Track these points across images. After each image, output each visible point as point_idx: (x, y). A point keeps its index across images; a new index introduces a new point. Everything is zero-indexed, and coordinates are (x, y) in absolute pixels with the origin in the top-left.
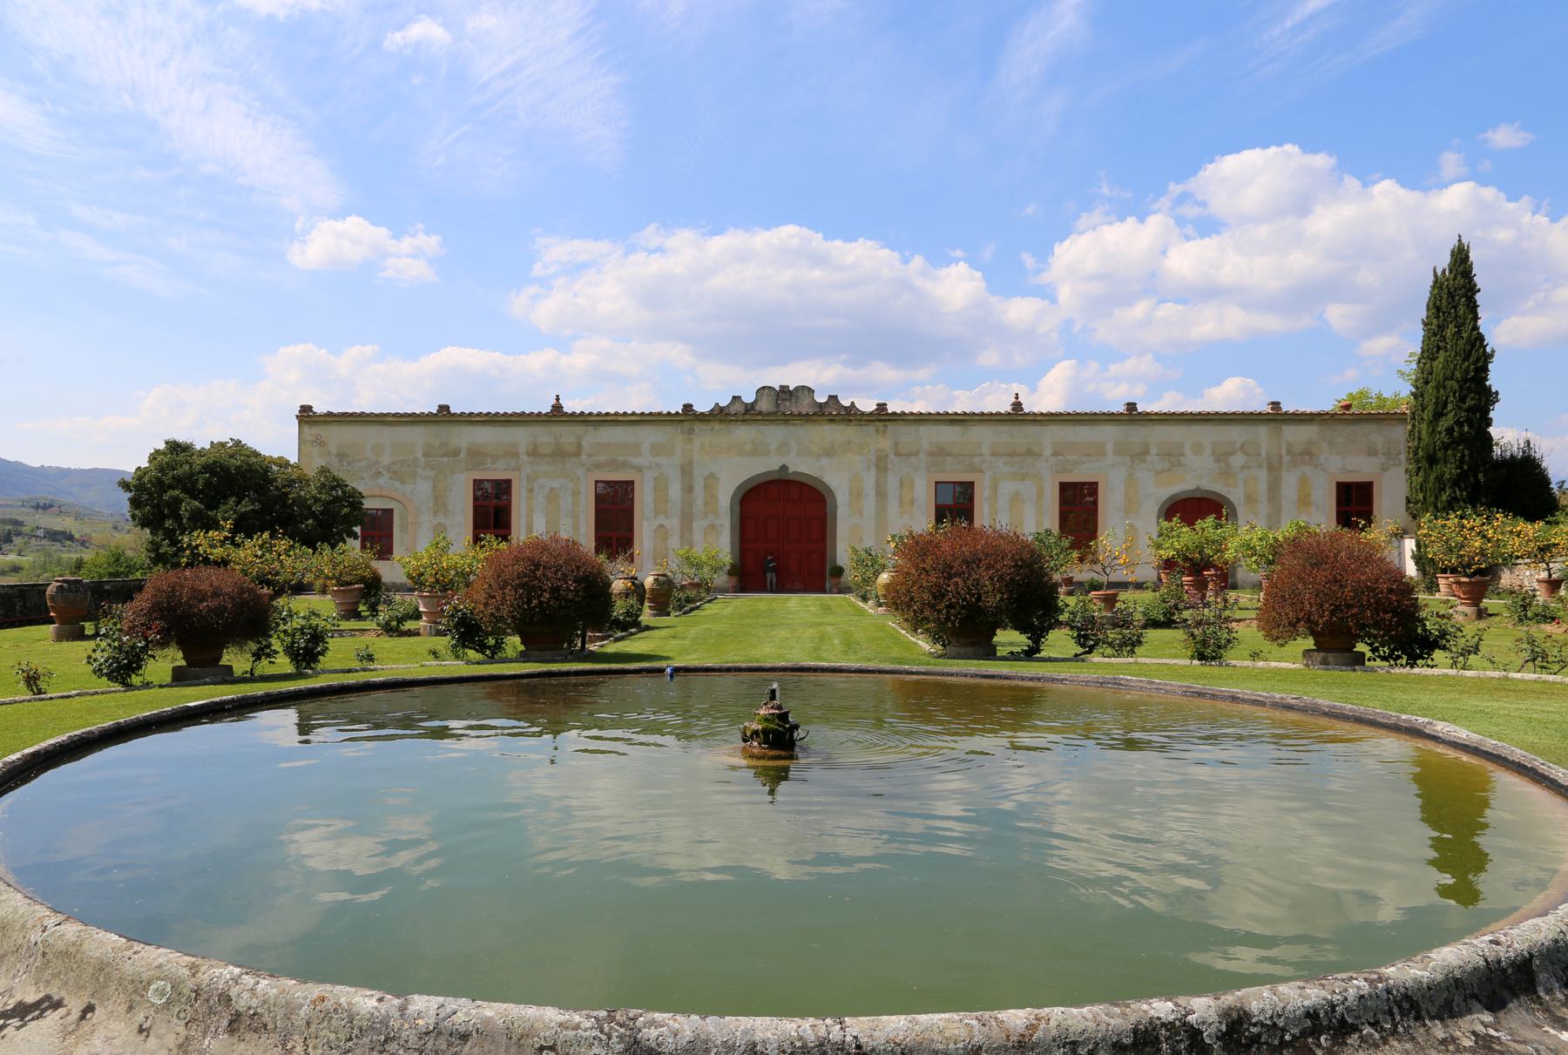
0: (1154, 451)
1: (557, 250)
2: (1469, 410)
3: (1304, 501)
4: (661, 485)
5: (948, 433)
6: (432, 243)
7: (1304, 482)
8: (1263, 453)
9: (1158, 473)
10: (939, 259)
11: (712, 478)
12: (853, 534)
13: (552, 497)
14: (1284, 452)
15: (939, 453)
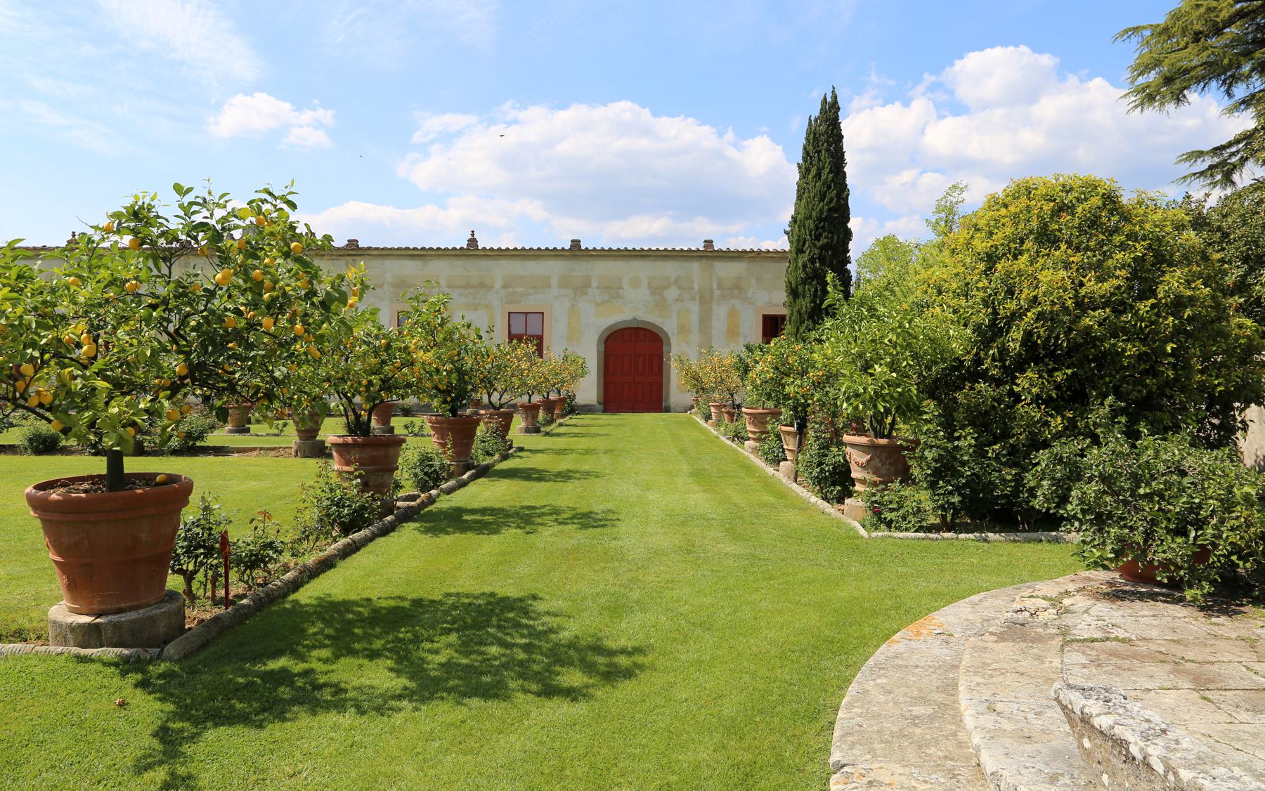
0: (595, 284)
1: (433, 123)
2: (822, 248)
5: (410, 268)
6: (327, 116)
7: (732, 314)
8: (696, 287)
9: (598, 305)
10: (746, 132)
12: (683, 358)
14: (715, 286)
15: (401, 284)
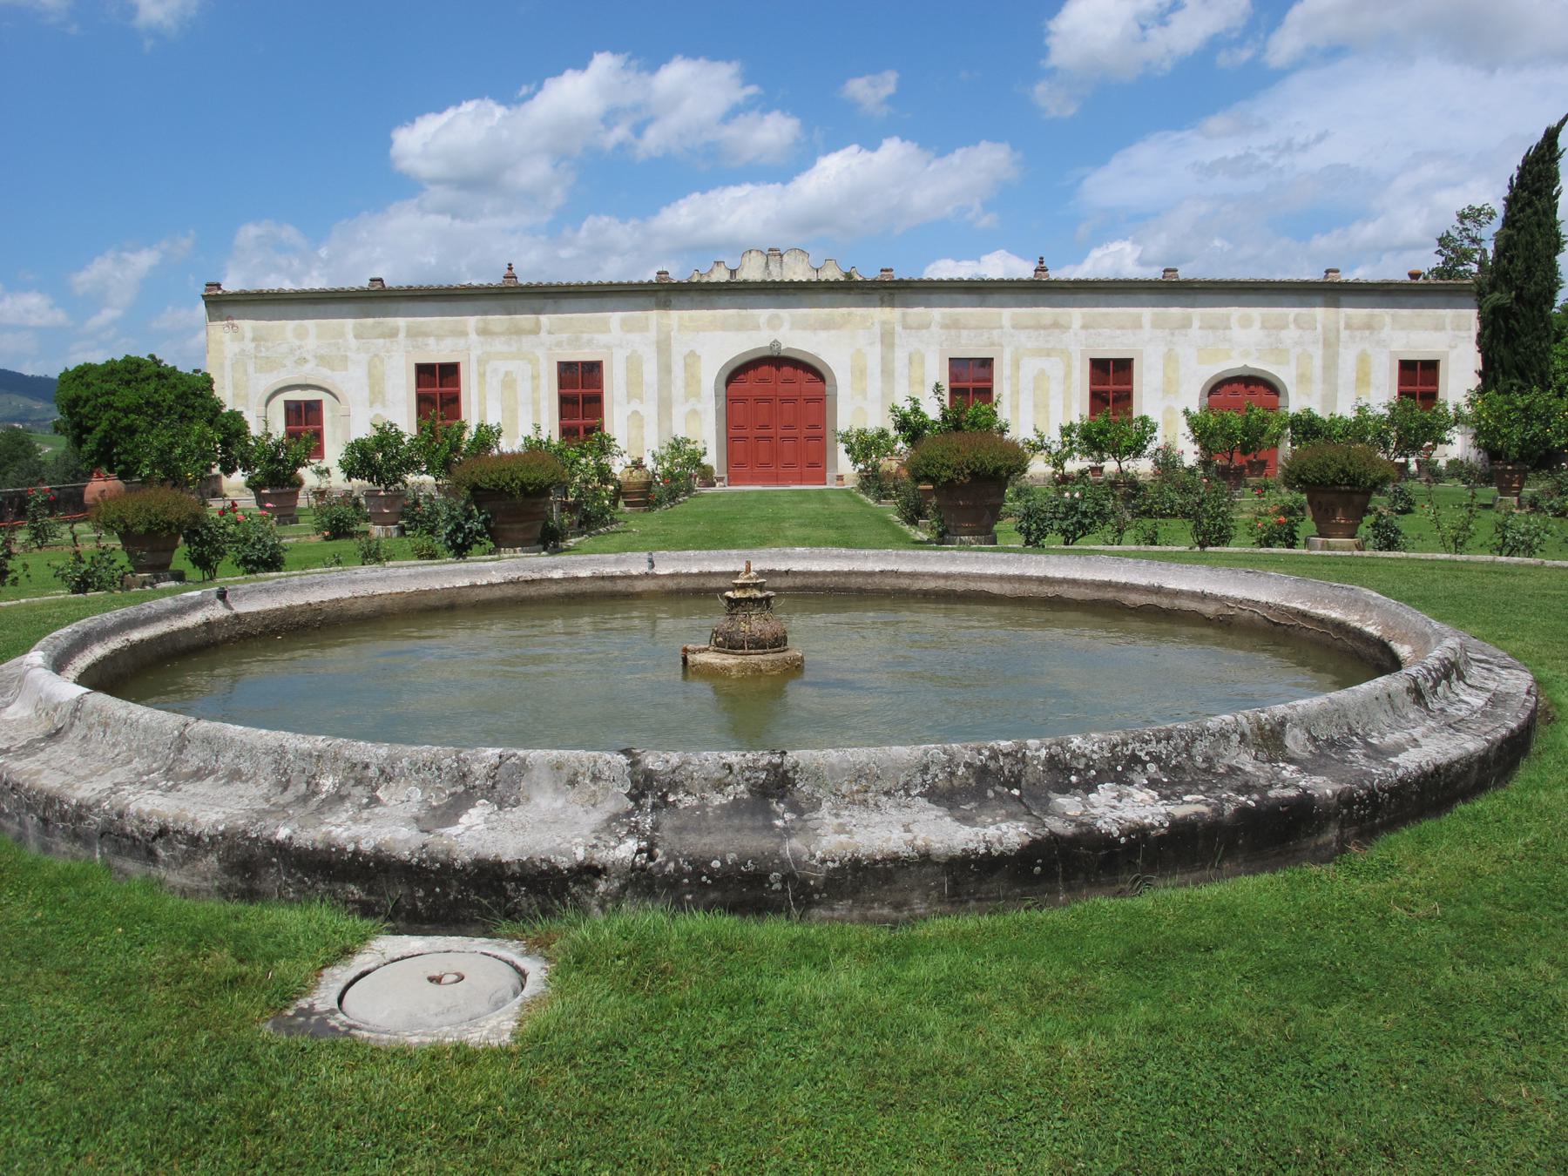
3: (1363, 380)
4: (634, 364)
7: (1363, 360)
11: (692, 358)
13: (508, 383)
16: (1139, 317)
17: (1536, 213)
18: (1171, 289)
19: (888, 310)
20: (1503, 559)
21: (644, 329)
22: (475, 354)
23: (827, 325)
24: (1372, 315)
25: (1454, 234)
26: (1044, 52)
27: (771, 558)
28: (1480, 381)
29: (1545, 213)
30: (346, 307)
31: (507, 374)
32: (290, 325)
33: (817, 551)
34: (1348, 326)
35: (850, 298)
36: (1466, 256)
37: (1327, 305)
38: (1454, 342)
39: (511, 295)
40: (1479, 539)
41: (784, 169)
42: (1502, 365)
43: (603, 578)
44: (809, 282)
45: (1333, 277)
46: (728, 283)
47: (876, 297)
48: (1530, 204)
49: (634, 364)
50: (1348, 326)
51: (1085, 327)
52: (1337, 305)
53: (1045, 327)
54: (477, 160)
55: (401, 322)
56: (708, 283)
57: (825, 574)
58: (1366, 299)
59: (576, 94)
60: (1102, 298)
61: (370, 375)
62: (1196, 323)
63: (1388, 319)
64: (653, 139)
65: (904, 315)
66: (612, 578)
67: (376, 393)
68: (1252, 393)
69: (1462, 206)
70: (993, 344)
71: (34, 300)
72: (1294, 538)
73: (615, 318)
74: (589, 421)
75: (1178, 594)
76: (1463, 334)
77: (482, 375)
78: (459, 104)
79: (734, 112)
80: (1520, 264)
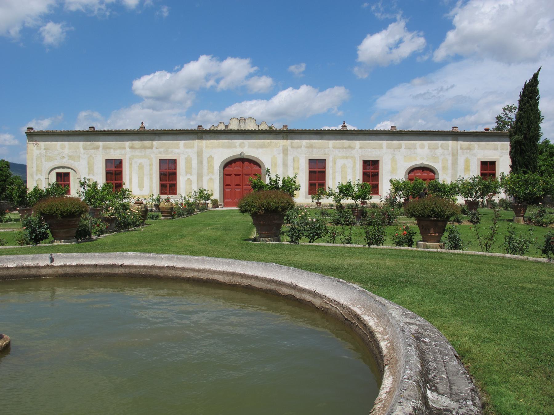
4: (188, 161)
7: (467, 161)
11: (210, 158)
13: (141, 167)
16: (382, 144)
17: (530, 105)
18: (394, 134)
19: (285, 141)
20: (509, 255)
21: (193, 147)
22: (128, 156)
23: (262, 147)
24: (470, 145)
25: (502, 115)
26: (356, 56)
27: (115, 257)
28: (511, 169)
29: (534, 105)
30: (80, 138)
31: (140, 164)
32: (58, 144)
33: (138, 254)
34: (461, 148)
35: (271, 136)
36: (505, 123)
37: (453, 140)
38: (501, 154)
39: (143, 134)
40: (498, 243)
41: (268, 96)
42: (519, 163)
43: (23, 267)
44: (255, 130)
45: (455, 130)
46: (224, 130)
47: (281, 136)
48: (528, 102)
49: (188, 161)
50: (461, 148)
51: (361, 148)
52: (457, 140)
53: (345, 148)
54: (161, 90)
55: (101, 143)
56: (217, 130)
57: (140, 267)
58: (468, 138)
59: (196, 69)
60: (367, 137)
61: (88, 163)
62: (403, 147)
63: (476, 146)
64: (222, 85)
65: (291, 143)
66: (28, 268)
67: (91, 169)
68: (425, 173)
69: (504, 106)
70: (325, 154)
71: (7, 136)
72: (413, 242)
73: (182, 143)
74: (171, 182)
75: (303, 290)
76: (504, 151)
77: (131, 164)
78: (155, 72)
79: (250, 76)
80: (525, 125)
